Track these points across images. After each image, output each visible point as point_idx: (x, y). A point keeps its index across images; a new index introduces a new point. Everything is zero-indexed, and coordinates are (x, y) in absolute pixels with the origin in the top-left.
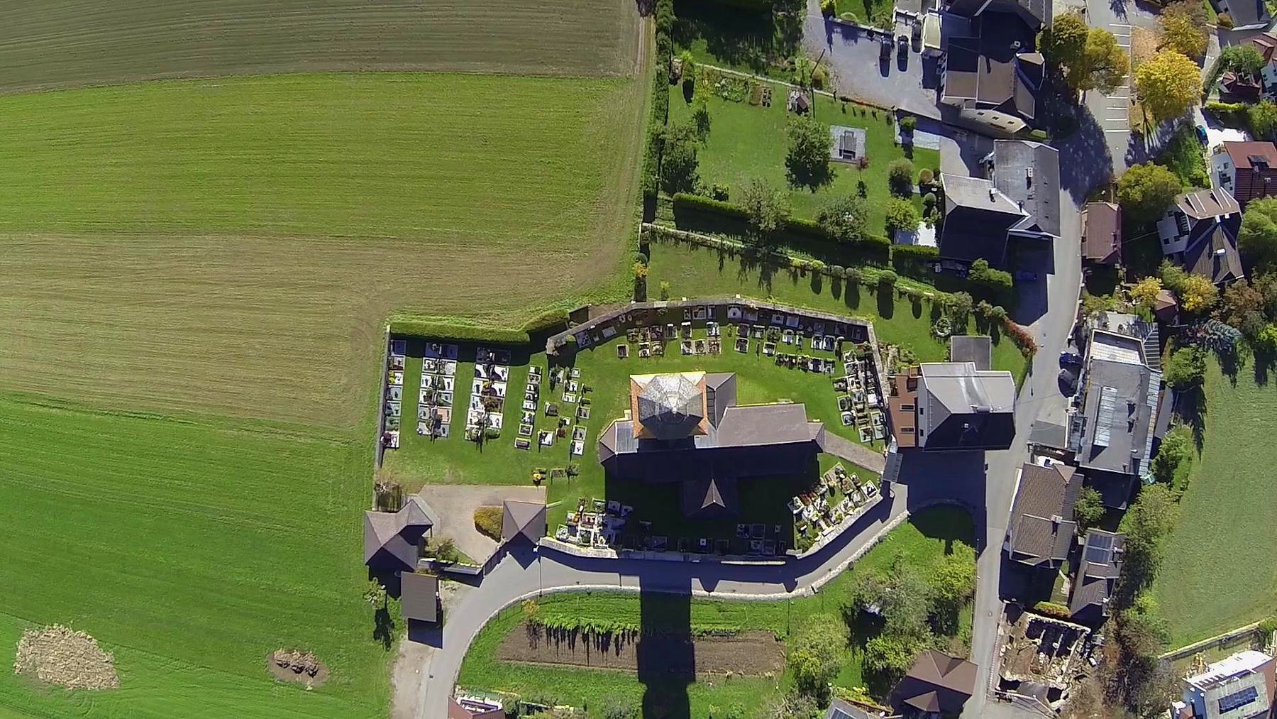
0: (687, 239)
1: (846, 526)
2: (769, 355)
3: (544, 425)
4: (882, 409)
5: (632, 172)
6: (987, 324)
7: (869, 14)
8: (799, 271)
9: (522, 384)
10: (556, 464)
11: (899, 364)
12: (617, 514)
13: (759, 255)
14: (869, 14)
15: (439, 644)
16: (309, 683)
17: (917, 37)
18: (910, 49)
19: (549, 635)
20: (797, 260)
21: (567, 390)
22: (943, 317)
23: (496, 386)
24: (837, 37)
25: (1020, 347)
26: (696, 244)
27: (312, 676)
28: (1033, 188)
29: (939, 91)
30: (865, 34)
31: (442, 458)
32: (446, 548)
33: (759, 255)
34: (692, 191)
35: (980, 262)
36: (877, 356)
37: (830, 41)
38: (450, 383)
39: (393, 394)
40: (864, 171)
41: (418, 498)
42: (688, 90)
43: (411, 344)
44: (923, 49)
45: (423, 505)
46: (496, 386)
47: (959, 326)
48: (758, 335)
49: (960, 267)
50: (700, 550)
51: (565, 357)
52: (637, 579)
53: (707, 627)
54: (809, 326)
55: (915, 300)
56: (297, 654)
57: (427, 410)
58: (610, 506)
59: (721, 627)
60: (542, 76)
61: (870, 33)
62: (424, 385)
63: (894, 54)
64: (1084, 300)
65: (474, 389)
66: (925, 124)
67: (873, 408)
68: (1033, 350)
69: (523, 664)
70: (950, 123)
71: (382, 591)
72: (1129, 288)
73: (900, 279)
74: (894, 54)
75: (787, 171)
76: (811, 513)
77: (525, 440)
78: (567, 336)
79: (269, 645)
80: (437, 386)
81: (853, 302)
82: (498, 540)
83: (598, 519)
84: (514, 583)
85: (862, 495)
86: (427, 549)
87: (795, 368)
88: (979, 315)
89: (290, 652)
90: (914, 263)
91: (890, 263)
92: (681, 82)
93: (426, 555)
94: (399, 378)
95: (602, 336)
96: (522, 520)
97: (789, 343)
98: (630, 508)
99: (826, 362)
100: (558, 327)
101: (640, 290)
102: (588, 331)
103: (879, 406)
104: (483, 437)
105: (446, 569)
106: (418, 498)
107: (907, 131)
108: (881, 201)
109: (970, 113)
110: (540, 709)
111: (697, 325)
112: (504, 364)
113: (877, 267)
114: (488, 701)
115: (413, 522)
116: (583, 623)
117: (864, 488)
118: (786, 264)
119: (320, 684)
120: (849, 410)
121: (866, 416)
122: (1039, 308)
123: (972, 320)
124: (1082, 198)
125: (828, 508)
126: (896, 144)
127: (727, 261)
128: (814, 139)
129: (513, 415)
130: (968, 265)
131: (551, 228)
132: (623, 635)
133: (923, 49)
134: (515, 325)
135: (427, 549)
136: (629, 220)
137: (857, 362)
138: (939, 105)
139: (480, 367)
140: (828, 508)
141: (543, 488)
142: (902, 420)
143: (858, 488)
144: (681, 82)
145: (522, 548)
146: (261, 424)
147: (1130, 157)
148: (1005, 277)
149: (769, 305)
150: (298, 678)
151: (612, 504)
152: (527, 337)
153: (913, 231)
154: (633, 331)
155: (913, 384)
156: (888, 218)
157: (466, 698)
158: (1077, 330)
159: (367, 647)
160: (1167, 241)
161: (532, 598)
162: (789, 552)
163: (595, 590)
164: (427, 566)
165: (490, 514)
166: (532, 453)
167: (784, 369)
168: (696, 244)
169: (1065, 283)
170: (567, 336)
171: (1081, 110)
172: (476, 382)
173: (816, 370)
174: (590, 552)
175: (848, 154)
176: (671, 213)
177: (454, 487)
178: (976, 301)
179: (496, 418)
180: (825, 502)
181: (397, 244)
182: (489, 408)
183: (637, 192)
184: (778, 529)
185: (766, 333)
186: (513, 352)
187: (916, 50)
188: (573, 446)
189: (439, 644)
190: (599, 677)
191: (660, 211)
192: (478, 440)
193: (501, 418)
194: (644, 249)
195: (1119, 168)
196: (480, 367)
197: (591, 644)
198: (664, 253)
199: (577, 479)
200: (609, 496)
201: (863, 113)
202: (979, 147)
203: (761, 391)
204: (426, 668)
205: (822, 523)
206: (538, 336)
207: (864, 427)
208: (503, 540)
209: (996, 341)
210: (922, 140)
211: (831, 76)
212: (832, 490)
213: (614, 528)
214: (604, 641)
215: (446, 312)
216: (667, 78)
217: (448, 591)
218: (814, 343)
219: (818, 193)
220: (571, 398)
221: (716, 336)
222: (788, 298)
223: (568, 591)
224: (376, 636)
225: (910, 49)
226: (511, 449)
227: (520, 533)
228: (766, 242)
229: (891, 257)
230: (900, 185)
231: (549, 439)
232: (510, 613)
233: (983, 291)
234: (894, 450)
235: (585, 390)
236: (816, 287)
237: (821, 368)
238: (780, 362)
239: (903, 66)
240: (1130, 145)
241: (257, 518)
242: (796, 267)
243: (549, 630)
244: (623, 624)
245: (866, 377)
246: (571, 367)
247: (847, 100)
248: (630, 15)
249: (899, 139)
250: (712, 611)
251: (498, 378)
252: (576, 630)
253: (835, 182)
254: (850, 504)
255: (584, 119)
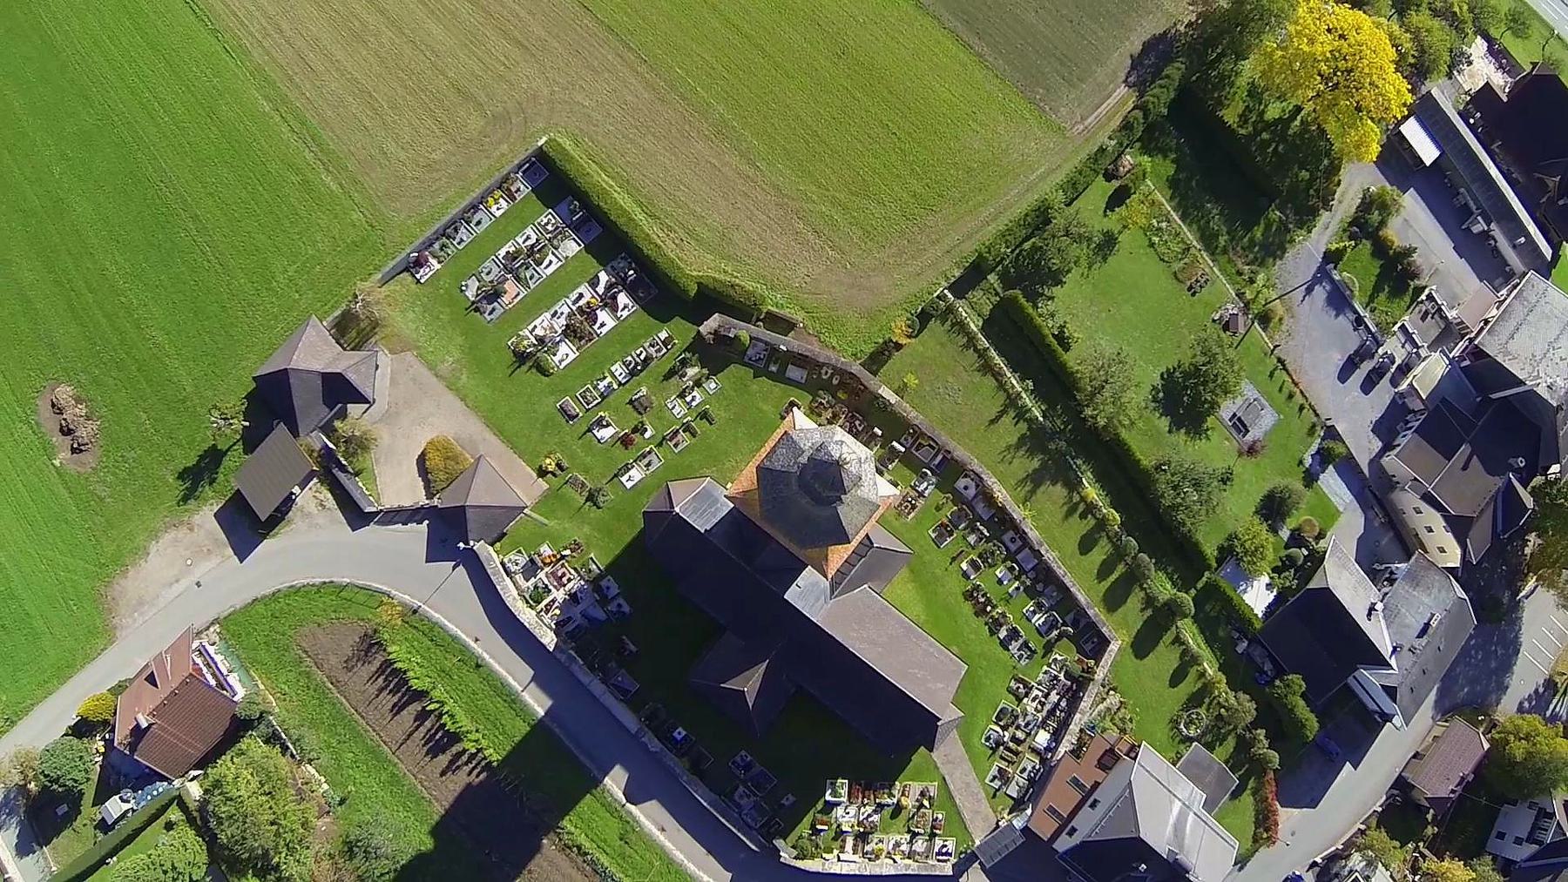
0: (982, 354)
1: (877, 871)
2: (965, 575)
3: (616, 410)
4: (1043, 761)
5: (985, 223)
6: (1245, 762)
7: (1372, 299)
8: (1082, 507)
9: (636, 341)
10: (586, 471)
11: (1108, 724)
12: (604, 600)
13: (1052, 446)
14: (1372, 299)
15: (242, 552)
16: (63, 456)
17: (1405, 369)
18: (1389, 375)
19: (381, 670)
20: (1092, 491)
21: (682, 396)
22: (1202, 711)
23: (603, 316)
24: (1320, 293)
25: (1257, 824)
26: (987, 368)
27: (74, 451)
28: (1424, 641)
29: (1387, 447)
30: (1353, 317)
31: (460, 340)
32: (358, 445)
33: (1052, 446)
34: (1036, 307)
35: (1297, 681)
36: (1093, 690)
37: (1309, 290)
38: (551, 265)
39: (477, 218)
40: (1245, 459)
41: (384, 358)
42: (1118, 199)
43: (551, 180)
44: (1404, 386)
45: (381, 372)
46: (603, 316)
47: (1209, 738)
48: (972, 539)
49: (1268, 667)
50: (666, 737)
51: (715, 355)
52: (549, 703)
53: (587, 845)
54: (1041, 581)
55: (1188, 660)
56: (82, 410)
57: (495, 270)
58: (604, 583)
59: (605, 860)
60: (968, 46)
61: (1359, 321)
62: (520, 241)
63: (1367, 366)
64: (1369, 828)
65: (574, 296)
66: (1348, 469)
67: (1034, 750)
68: (1271, 841)
69: (319, 676)
70: (1374, 491)
71: (239, 424)
72: (1424, 857)
73: (1188, 621)
74: (1367, 366)
75: (1158, 382)
76: (847, 816)
77: (575, 408)
78: (743, 331)
79: (65, 370)
80: (535, 254)
81: (1113, 601)
82: (430, 496)
83: (573, 585)
84: (395, 563)
85: (929, 849)
86: (337, 424)
87: (982, 620)
88: (1244, 745)
89: (78, 401)
90: (1220, 616)
91: (1193, 592)
92: (1116, 184)
93: (328, 430)
94: (500, 207)
95: (782, 370)
96: (479, 495)
97: (1000, 582)
98: (626, 608)
99: (1025, 645)
100: (742, 309)
101: (878, 359)
102: (773, 350)
103: (1043, 755)
104: (528, 360)
105: (341, 476)
106: (384, 358)
107: (1324, 458)
108: (1236, 511)
109: (1408, 501)
110: (285, 749)
111: (908, 460)
112: (636, 299)
113: (1174, 584)
114: (233, 679)
115: (352, 377)
116: (435, 694)
117: (938, 842)
118: (1073, 485)
119: (72, 469)
120: (1004, 728)
121: (1016, 753)
122: (1310, 798)
123: (1231, 743)
124: (1447, 709)
125: (873, 829)
126: (1301, 462)
127: (1007, 420)
128: (1220, 366)
129: (591, 366)
130: (1280, 672)
131: (835, 202)
132: (473, 756)
133: (1404, 386)
134: (693, 264)
135: (337, 424)
136: (932, 276)
137: (1061, 676)
138: (1375, 462)
139: (604, 277)
140: (873, 829)
141: (543, 484)
142: (1059, 795)
143: (933, 836)
144: (1116, 184)
145: (449, 532)
146: (303, 124)
147: (1526, 705)
148: (1312, 723)
149: (1018, 513)
150: (57, 439)
151: (610, 583)
152: (693, 290)
153: (1248, 577)
154: (825, 398)
155: (1108, 760)
156: (1230, 538)
157: (211, 650)
158: (1333, 858)
159: (162, 479)
160: (1501, 836)
161: (402, 604)
162: (779, 843)
163: (487, 666)
164: (318, 446)
165: (450, 456)
166: (570, 431)
167: (967, 608)
168: (987, 368)
169: (1358, 789)
170: (743, 331)
171: (1516, 606)
172: (583, 288)
173: (1004, 644)
174: (526, 615)
175: (1240, 426)
176: (987, 310)
177: (439, 386)
178: (1255, 725)
179: (566, 352)
180: (876, 818)
181: (642, 69)
182: (571, 332)
183: (969, 251)
184: (789, 800)
185: (982, 546)
186: (659, 292)
187: (1394, 382)
188: (627, 468)
189: (242, 552)
190: (395, 780)
191: (977, 295)
192: (521, 357)
193: (572, 356)
194: (924, 318)
195: (1506, 709)
196: (604, 277)
197: (423, 730)
198: (942, 344)
199: (595, 513)
200: (613, 568)
201: (1291, 396)
202: (1389, 545)
203: (918, 610)
204: (203, 569)
205: (850, 842)
206: (709, 300)
207: (1003, 765)
208: (436, 501)
209: (1236, 795)
210: (1332, 483)
211: (1284, 328)
212: (898, 809)
213: (584, 615)
214: (442, 741)
215: (626, 184)
216: (1104, 164)
217: (313, 499)
218: (1030, 606)
219: (1173, 438)
220: (679, 410)
221: (921, 495)
222: (1045, 523)
223: (455, 638)
224: (182, 476)
225: (1389, 375)
226: (550, 404)
227: (463, 507)
228: (1071, 434)
229: (1200, 585)
230: (1273, 508)
231: (605, 433)
232: (361, 597)
233: (1274, 718)
234: (1018, 823)
235: (704, 415)
236: (1086, 545)
237: (1014, 646)
238: (969, 596)
239: (1368, 386)
240: (1536, 691)
241: (195, 218)
242: (1083, 499)
243: (388, 663)
244: (484, 743)
245: (1058, 704)
246: (714, 371)
247: (1285, 369)
248: (1114, 72)
249: (1308, 461)
250: (612, 829)
251: (614, 308)
252: (420, 695)
253: (1202, 444)
254: (904, 847)
255: (974, 125)
